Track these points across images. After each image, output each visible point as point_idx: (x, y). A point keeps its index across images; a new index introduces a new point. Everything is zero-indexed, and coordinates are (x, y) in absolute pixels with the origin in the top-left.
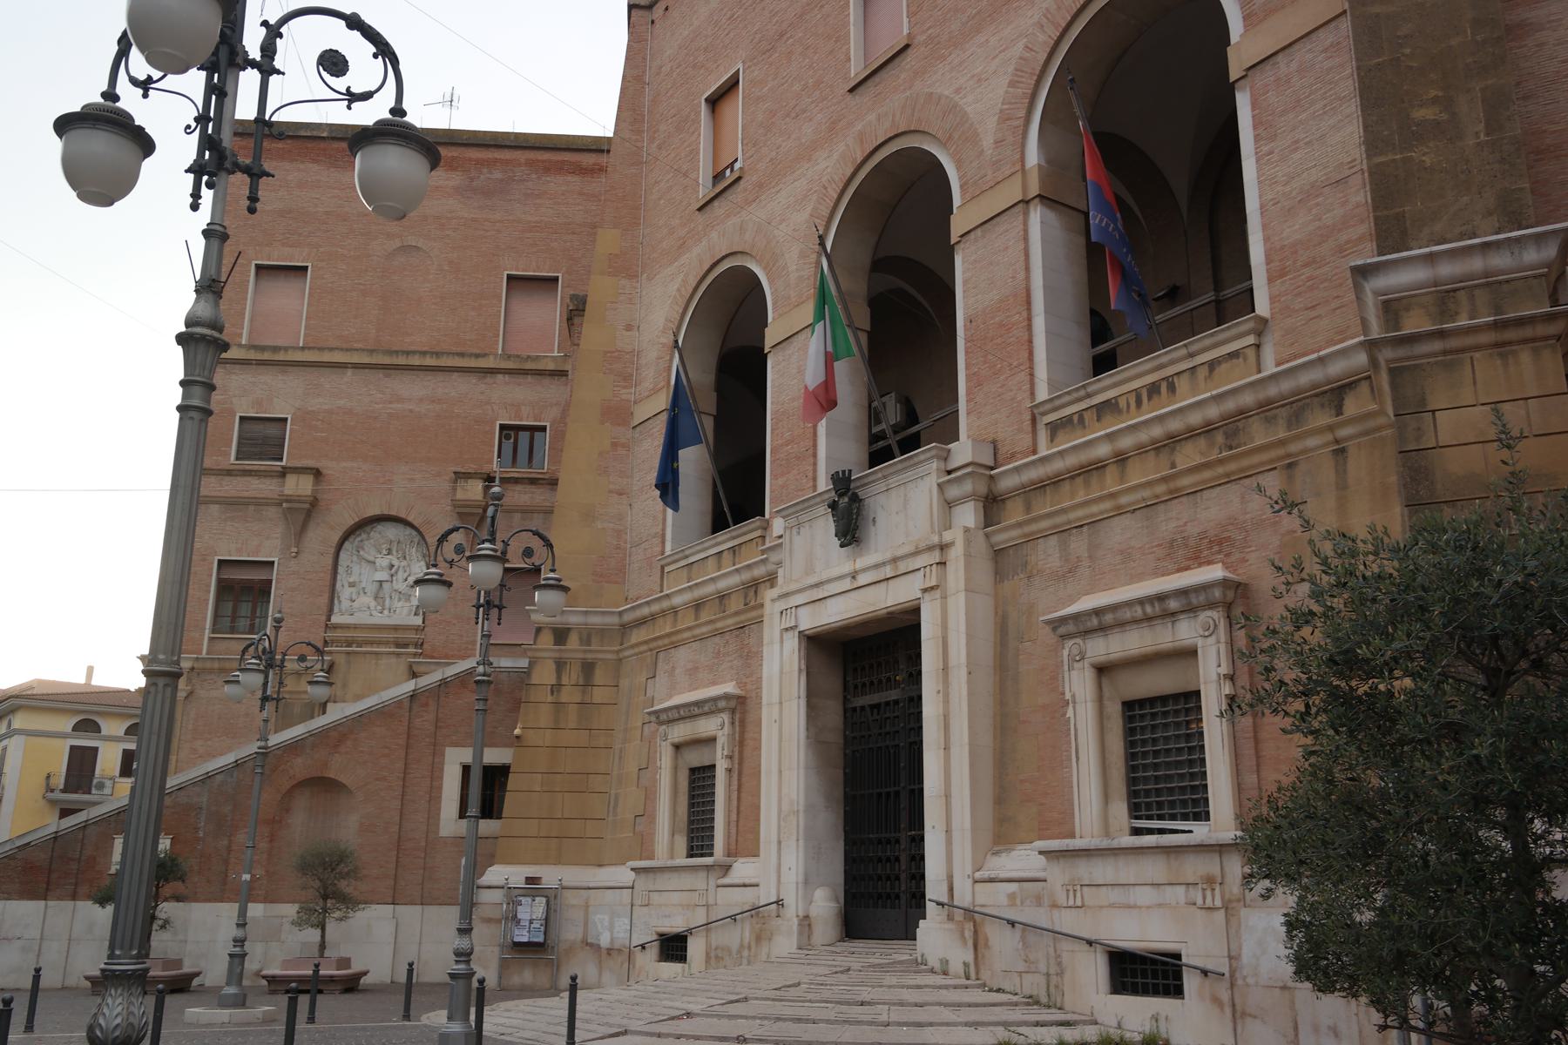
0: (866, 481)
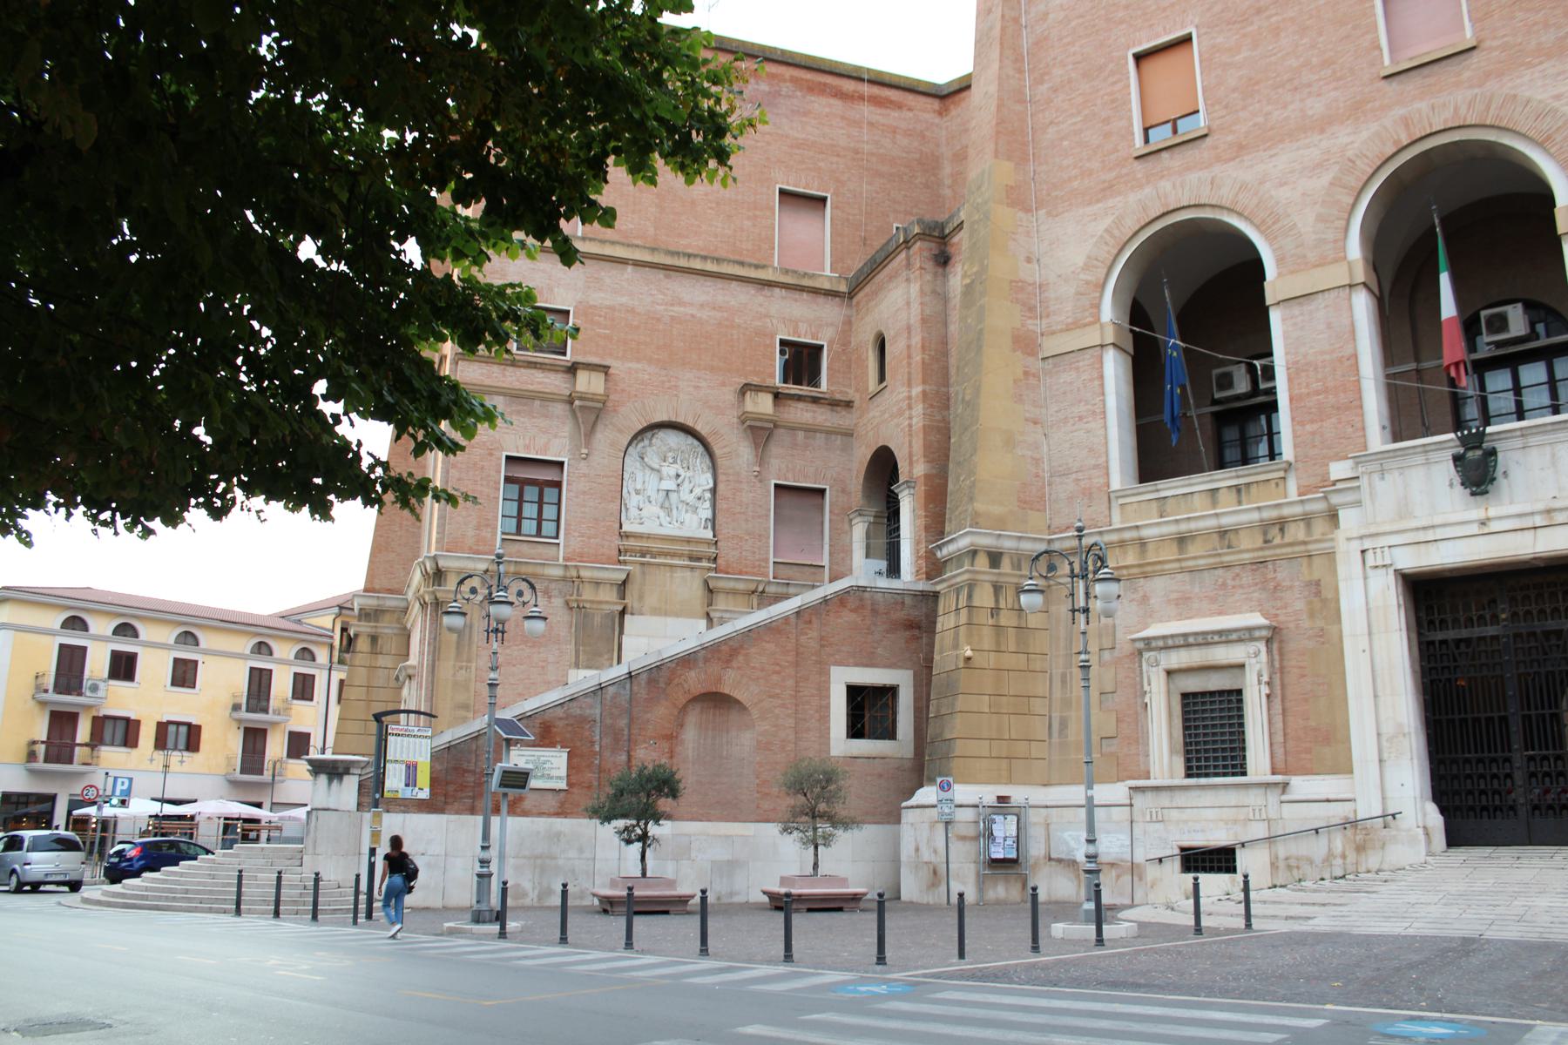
0: (1503, 436)
